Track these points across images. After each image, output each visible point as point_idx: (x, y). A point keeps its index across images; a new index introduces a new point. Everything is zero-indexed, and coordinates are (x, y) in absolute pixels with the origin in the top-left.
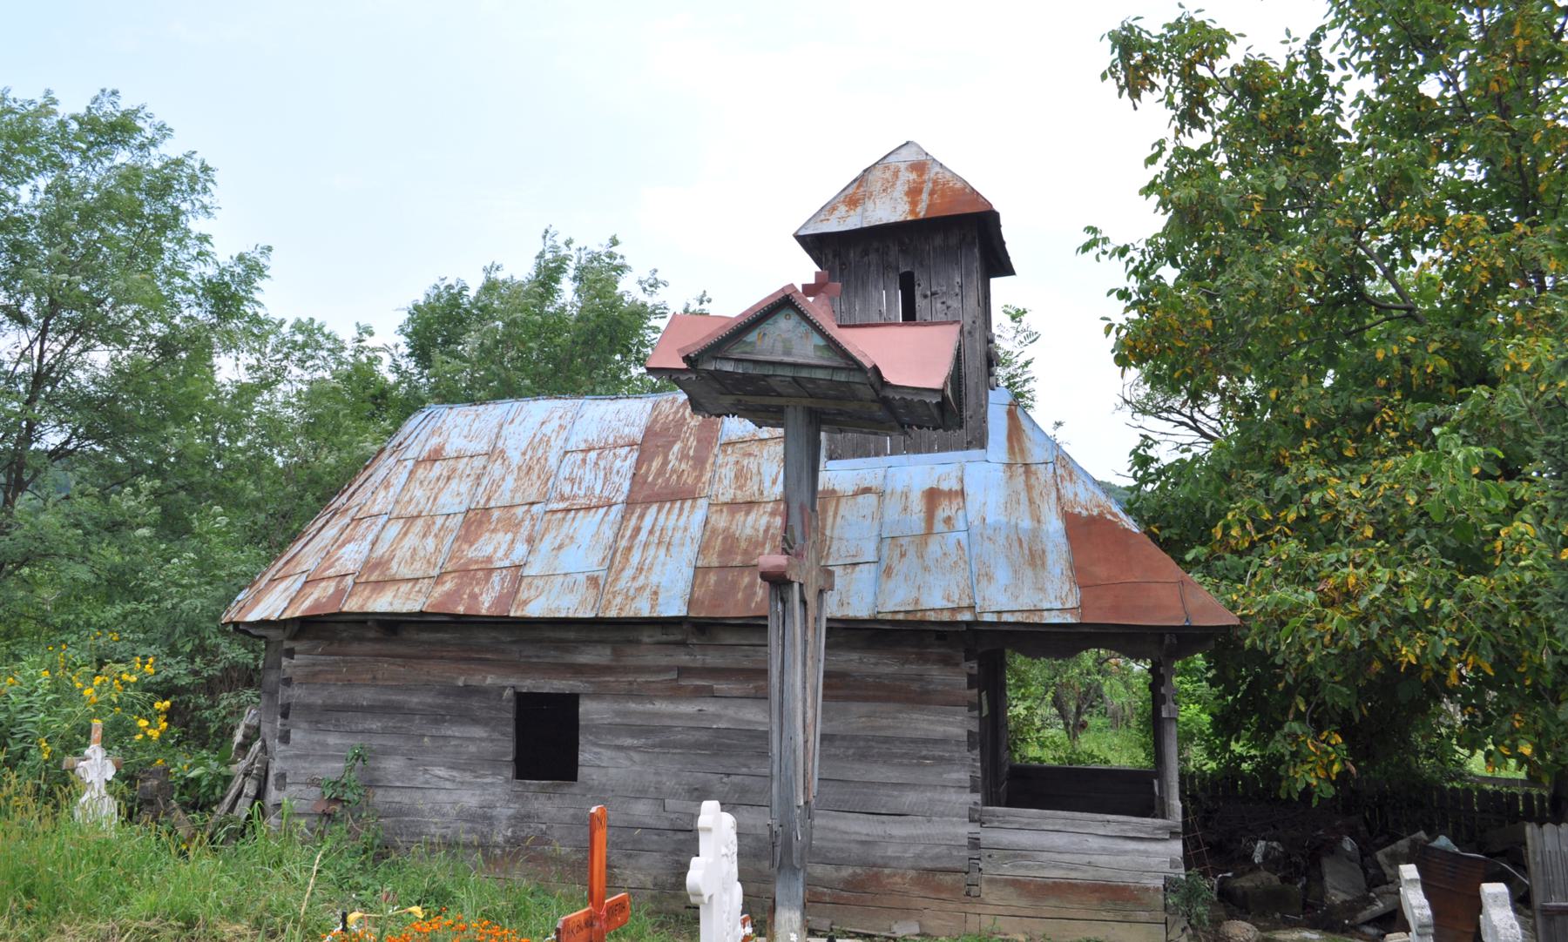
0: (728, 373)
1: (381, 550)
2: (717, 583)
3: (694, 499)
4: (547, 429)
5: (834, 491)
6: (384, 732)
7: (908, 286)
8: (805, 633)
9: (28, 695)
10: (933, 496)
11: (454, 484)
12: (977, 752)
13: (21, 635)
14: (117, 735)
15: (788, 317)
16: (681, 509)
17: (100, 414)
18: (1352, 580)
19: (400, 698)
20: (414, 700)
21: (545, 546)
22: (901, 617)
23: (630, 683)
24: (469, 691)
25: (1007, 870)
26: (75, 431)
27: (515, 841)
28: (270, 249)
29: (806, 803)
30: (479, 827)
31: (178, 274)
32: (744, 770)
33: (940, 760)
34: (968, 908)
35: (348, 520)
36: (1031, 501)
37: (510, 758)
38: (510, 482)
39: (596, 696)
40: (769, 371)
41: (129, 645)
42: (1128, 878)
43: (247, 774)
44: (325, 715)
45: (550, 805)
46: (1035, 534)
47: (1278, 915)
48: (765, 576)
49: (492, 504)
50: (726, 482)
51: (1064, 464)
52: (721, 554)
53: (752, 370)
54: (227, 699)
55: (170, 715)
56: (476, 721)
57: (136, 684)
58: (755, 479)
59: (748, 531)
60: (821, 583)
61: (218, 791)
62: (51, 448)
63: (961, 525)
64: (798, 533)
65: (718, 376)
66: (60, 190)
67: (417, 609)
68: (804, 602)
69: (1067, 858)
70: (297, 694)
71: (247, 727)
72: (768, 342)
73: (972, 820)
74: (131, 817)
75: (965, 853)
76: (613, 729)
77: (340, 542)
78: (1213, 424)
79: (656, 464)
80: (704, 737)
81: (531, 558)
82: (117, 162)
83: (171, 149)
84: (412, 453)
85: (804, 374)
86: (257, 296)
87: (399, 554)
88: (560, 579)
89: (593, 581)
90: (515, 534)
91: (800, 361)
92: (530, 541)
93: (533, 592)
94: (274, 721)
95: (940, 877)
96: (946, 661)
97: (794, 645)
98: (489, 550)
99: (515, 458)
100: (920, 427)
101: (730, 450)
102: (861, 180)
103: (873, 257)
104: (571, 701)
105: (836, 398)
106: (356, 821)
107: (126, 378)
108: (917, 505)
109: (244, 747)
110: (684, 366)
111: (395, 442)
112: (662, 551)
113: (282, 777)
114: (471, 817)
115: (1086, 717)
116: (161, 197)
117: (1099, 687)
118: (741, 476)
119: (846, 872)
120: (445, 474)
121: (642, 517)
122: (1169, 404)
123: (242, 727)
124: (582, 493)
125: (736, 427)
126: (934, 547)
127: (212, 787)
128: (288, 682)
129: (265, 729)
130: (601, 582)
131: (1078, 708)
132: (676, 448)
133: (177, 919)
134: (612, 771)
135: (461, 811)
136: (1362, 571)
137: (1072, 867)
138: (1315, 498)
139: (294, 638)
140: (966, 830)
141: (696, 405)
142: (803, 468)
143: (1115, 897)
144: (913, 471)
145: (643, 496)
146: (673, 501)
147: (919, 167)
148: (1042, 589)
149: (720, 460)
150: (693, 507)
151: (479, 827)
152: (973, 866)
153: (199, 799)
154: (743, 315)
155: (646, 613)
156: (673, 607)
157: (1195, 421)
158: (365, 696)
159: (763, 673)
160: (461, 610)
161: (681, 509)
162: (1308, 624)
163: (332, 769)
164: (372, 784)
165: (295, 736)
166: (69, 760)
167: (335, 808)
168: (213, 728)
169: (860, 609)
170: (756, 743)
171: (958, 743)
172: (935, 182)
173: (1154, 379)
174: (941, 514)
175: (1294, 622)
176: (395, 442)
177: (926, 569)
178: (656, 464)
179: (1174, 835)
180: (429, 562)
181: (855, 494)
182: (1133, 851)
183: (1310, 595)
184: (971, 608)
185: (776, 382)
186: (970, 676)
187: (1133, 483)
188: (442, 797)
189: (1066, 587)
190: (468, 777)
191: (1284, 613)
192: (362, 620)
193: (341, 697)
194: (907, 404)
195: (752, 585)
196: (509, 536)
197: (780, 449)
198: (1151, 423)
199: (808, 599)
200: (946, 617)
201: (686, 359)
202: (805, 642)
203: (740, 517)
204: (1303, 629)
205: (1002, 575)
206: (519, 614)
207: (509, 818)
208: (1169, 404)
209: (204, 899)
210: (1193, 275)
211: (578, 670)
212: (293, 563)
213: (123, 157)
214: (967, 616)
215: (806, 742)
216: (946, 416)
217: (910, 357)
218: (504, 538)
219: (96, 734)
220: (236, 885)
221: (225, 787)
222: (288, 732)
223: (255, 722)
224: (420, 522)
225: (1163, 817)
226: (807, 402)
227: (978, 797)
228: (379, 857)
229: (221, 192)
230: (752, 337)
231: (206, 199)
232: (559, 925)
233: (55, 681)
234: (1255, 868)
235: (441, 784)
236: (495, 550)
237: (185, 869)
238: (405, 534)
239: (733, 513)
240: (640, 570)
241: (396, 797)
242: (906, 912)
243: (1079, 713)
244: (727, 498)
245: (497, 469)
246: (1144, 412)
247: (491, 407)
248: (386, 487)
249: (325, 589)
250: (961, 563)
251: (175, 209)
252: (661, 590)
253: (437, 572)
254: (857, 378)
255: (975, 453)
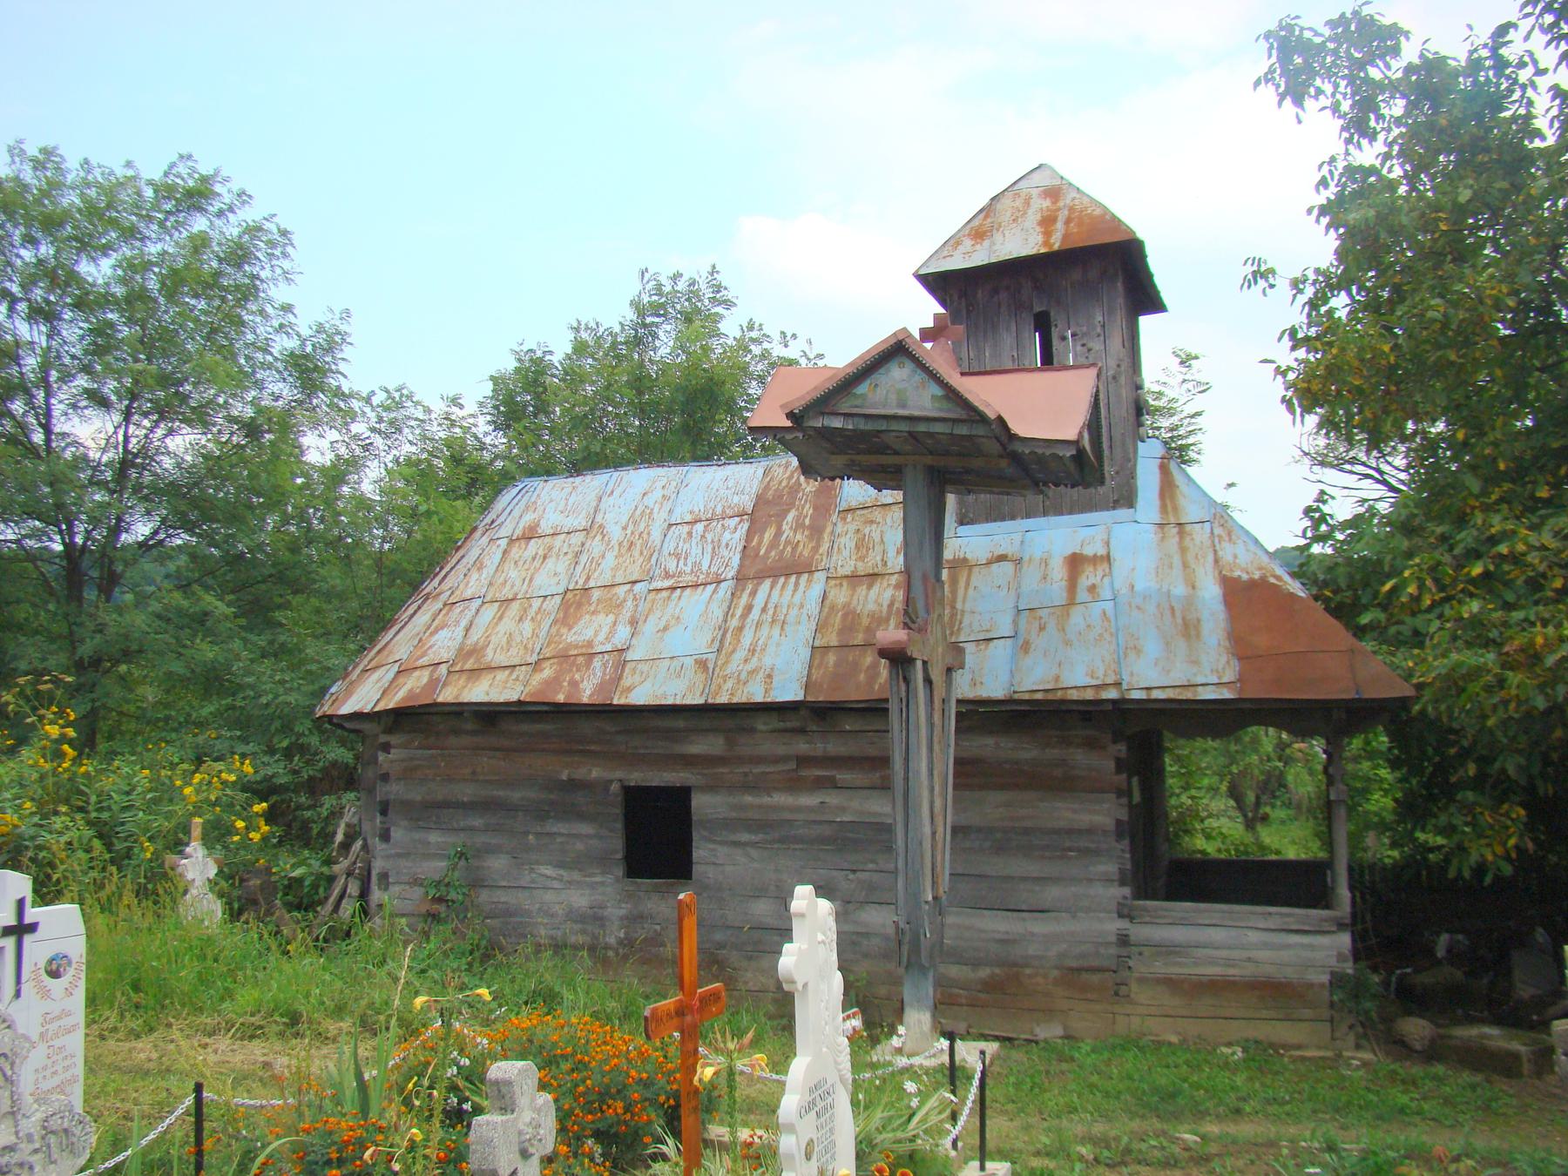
0: (841, 433)
1: (475, 636)
2: (837, 665)
3: (811, 572)
4: (649, 501)
5: (965, 560)
6: (486, 829)
7: (1043, 325)
8: (930, 716)
9: (128, 793)
10: (1075, 562)
11: (550, 563)
12: (1126, 842)
13: (122, 733)
14: (216, 835)
15: (902, 365)
16: (797, 584)
17: (185, 500)
18: (1539, 640)
19: (501, 793)
20: (516, 795)
21: (649, 628)
22: (1039, 696)
23: (746, 774)
24: (574, 785)
25: (1160, 968)
26: (164, 521)
27: (628, 942)
28: (347, 311)
29: (935, 898)
30: (589, 928)
31: (260, 349)
32: (871, 866)
33: (1085, 852)
34: (1117, 1009)
35: (440, 605)
36: (1185, 565)
37: (620, 856)
38: (610, 560)
39: (711, 788)
40: (883, 426)
41: (227, 744)
42: (1290, 974)
43: (349, 874)
44: (428, 812)
45: (662, 903)
46: (1190, 601)
47: (1460, 1012)
48: (883, 653)
49: (592, 584)
50: (846, 553)
51: (1220, 516)
52: (841, 632)
53: (863, 425)
54: (329, 802)
55: (270, 817)
56: (582, 817)
57: (234, 783)
58: (878, 548)
59: (871, 606)
60: (949, 660)
61: (321, 890)
62: (141, 538)
63: (1107, 594)
64: (920, 605)
65: (826, 434)
66: (135, 267)
67: (514, 697)
68: (928, 681)
69: (1224, 953)
70: (394, 790)
71: (348, 825)
72: (880, 393)
73: (1121, 916)
74: (234, 915)
75: (1113, 951)
76: (729, 824)
77: (432, 629)
78: (1403, 476)
79: (769, 535)
80: (827, 831)
81: (634, 642)
82: (195, 230)
83: (248, 215)
84: (505, 531)
85: (922, 428)
86: (342, 367)
87: (494, 639)
88: (666, 663)
89: (702, 664)
90: (617, 616)
91: (916, 413)
92: (633, 622)
93: (637, 678)
94: (374, 817)
95: (1085, 976)
96: (1091, 744)
97: (918, 726)
98: (588, 634)
99: (615, 533)
100: (1057, 485)
101: (849, 517)
102: (987, 210)
103: (1004, 296)
104: (682, 796)
105: (959, 454)
106: (462, 921)
107: (214, 466)
108: (1058, 572)
109: (346, 846)
110: (789, 424)
111: (488, 520)
112: (776, 630)
113: (384, 876)
114: (580, 918)
115: (1268, 809)
116: (239, 266)
117: (1282, 775)
118: (862, 545)
119: (984, 973)
120: (541, 552)
121: (753, 593)
122: (1352, 454)
123: (343, 826)
124: (688, 569)
125: (855, 491)
126: (1077, 617)
127: (315, 886)
128: (385, 777)
129: (366, 827)
130: (711, 666)
131: (1258, 798)
132: (790, 517)
133: (282, 1015)
134: (729, 869)
135: (571, 911)
136: (1550, 630)
137: (1230, 963)
138: (1503, 549)
139: (389, 731)
140: (1114, 926)
141: (807, 469)
142: (926, 535)
143: (1275, 993)
144: (1052, 536)
145: (756, 570)
146: (788, 575)
147: (1053, 193)
148: (1195, 662)
149: (839, 529)
150: (809, 581)
151: (589, 928)
152: (1122, 963)
153: (303, 899)
154: (851, 364)
155: (760, 700)
156: (789, 690)
157: (1381, 473)
158: (466, 792)
159: (883, 761)
160: (561, 698)
161: (797, 584)
162: (1488, 689)
163: (435, 868)
164: (476, 883)
165: (397, 834)
166: (170, 858)
167: (439, 909)
168: (316, 829)
169: (994, 687)
170: (877, 836)
171: (1105, 832)
172: (1071, 209)
173: (1328, 424)
174: (1085, 581)
175: (1474, 688)
176: (488, 520)
177: (1068, 643)
178: (769, 535)
179: (1341, 926)
180: (526, 647)
181: (989, 563)
182: (1302, 946)
183: (1490, 657)
184: (1118, 684)
185: (913, 446)
186: (1118, 761)
187: (1302, 542)
188: (549, 896)
189: (1224, 659)
190: (576, 876)
191: (1463, 677)
192: (458, 711)
193: (441, 792)
194: (1041, 460)
195: (875, 666)
196: (611, 618)
197: (898, 514)
198: (1330, 475)
199: (933, 677)
200: (1089, 695)
201: (790, 415)
202: (931, 725)
203: (862, 590)
204: (1483, 694)
205: (1152, 647)
206: (622, 701)
207: (621, 918)
208: (1352, 454)
209: (308, 995)
210: (1373, 306)
211: (689, 761)
212: (385, 653)
213: (200, 224)
214: (1112, 694)
215: (934, 834)
216: (1079, 473)
217: (1041, 404)
218: (605, 620)
219: (197, 832)
220: (339, 984)
221: (329, 887)
222: (388, 830)
223: (355, 820)
224: (515, 606)
225: (1328, 907)
226: (929, 460)
227: (1127, 891)
228: (486, 957)
229: (300, 256)
230: (862, 388)
231: (286, 264)
232: (647, 1013)
233: (155, 779)
234: (1439, 962)
235: (549, 883)
236: (596, 634)
237: (287, 967)
238: (501, 618)
239: (853, 588)
240: (752, 651)
241: (503, 897)
242: (1049, 1013)
243: (1258, 804)
244: (847, 571)
245: (596, 546)
246: (1322, 464)
247: (588, 478)
248: (479, 569)
249: (419, 678)
250: (1106, 636)
251: (255, 277)
252: (776, 672)
253: (534, 658)
254: (980, 430)
255: (1122, 513)
